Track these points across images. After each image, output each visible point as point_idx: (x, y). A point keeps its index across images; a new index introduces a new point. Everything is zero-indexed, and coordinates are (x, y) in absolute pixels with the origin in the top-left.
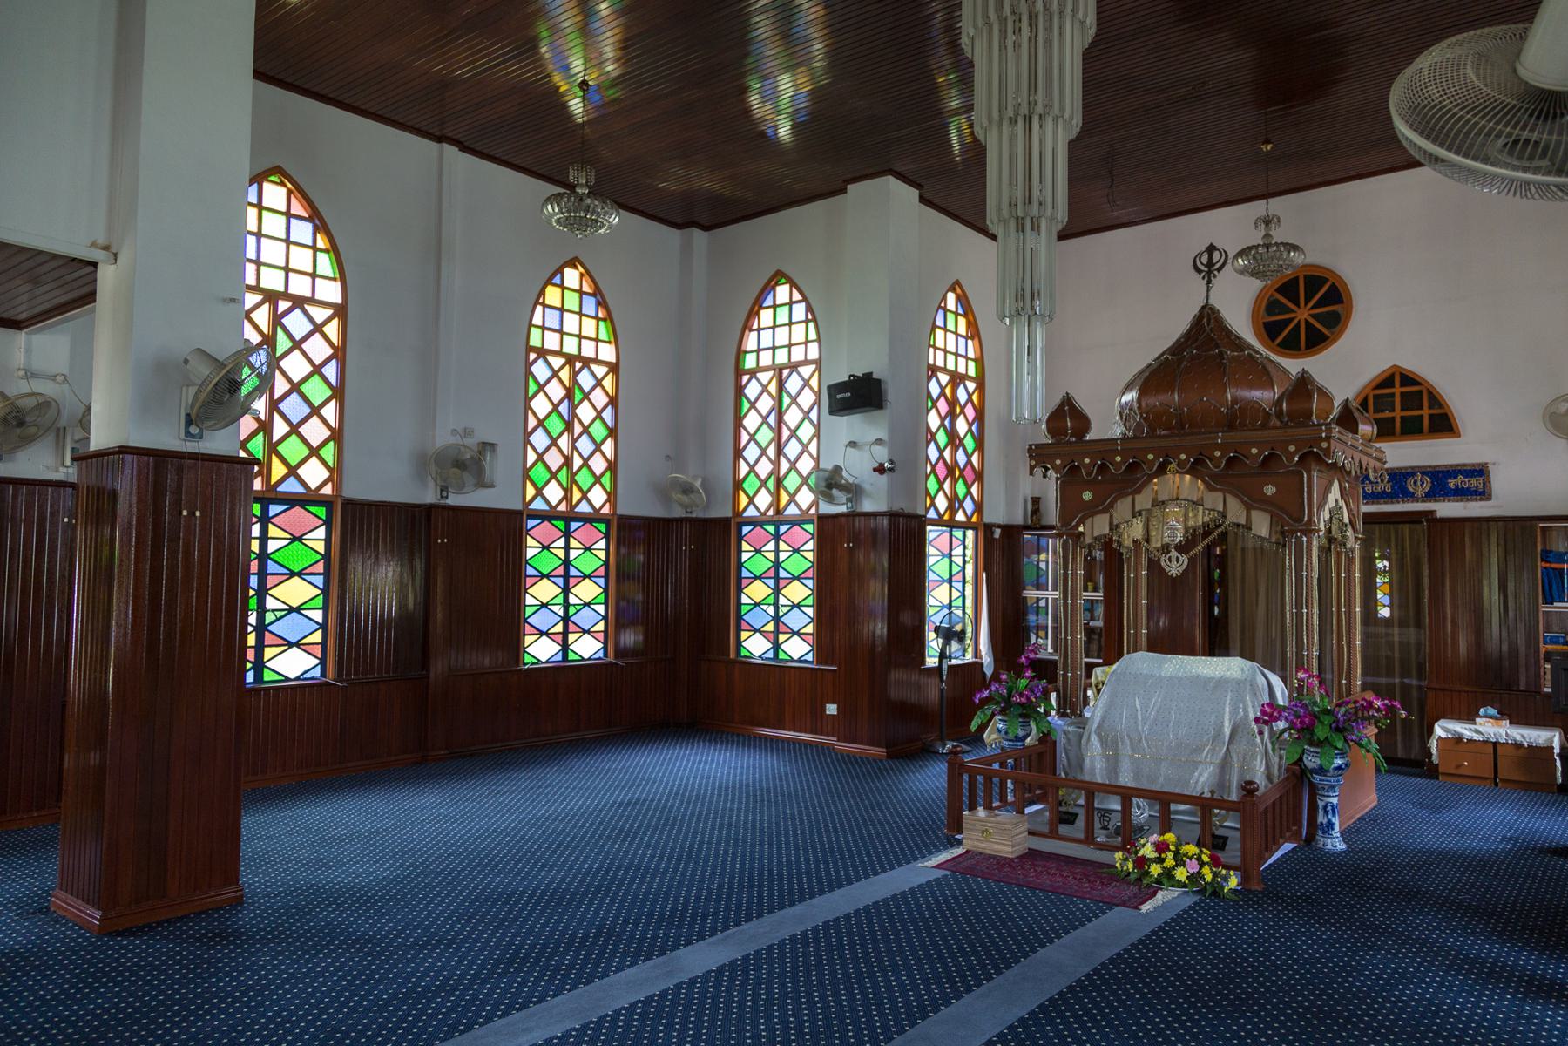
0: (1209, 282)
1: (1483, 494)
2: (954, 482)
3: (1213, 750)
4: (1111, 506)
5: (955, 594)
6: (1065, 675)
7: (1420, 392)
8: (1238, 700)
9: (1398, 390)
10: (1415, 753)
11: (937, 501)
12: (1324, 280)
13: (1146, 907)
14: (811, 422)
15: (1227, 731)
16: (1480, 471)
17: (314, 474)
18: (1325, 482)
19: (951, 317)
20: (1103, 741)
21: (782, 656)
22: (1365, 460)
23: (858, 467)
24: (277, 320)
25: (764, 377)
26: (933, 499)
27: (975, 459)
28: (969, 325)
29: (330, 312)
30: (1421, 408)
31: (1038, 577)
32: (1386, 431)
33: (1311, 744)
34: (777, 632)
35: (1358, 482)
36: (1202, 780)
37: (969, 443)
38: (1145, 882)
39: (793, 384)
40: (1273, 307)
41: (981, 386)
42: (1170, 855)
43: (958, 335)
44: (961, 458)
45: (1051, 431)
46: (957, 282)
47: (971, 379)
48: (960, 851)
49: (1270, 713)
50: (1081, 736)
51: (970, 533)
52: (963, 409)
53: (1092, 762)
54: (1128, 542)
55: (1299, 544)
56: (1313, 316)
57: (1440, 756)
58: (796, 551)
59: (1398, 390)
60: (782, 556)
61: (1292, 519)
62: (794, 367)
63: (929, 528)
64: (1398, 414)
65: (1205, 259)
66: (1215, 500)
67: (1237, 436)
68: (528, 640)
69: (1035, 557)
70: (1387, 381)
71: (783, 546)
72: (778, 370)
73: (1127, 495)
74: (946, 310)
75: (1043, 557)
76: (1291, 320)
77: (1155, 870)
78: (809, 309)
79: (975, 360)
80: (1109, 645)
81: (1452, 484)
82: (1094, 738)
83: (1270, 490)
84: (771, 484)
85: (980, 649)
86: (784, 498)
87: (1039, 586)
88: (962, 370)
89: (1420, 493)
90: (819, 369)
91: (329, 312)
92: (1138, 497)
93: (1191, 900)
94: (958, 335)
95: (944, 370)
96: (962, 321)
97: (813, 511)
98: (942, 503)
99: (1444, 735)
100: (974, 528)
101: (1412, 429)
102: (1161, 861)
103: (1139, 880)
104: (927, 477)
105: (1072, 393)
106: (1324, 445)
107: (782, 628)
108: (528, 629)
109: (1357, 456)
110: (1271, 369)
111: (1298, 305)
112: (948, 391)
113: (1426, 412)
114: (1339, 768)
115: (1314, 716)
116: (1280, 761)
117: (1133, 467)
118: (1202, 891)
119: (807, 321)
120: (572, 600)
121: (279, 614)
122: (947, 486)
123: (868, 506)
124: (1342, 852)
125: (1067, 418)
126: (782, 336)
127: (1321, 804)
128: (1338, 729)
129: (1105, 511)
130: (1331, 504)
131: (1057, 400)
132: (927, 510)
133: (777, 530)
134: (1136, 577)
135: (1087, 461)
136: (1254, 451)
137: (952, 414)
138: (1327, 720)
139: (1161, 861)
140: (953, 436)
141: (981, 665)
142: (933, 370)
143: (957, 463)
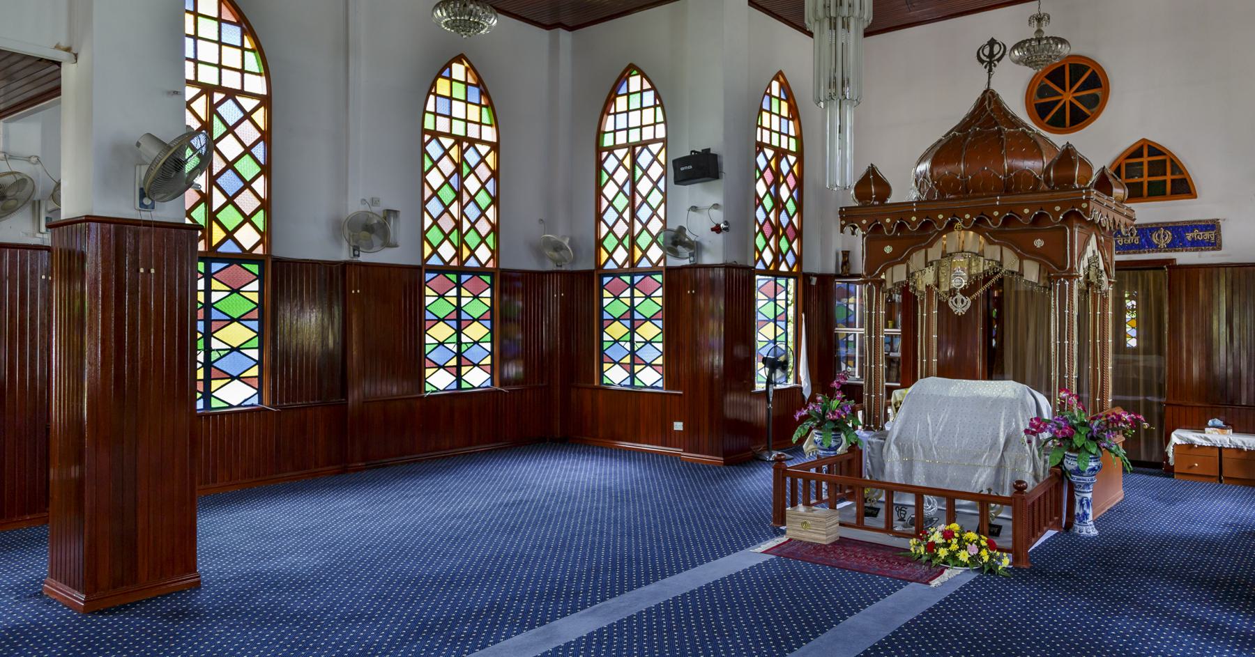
0: (990, 70)
1: (1216, 245)
2: (778, 239)
3: (990, 456)
4: (908, 257)
5: (779, 331)
6: (869, 397)
8: (1012, 415)
9: (1145, 159)
14: (659, 190)
15: (1002, 440)
16: (1213, 226)
17: (248, 237)
19: (775, 102)
21: (637, 383)
22: (1118, 217)
23: (699, 227)
24: (213, 109)
25: (620, 153)
26: (761, 254)
27: (795, 220)
29: (256, 102)
32: (1136, 193)
33: (1070, 450)
34: (633, 363)
35: (1110, 235)
36: (981, 480)
37: (791, 207)
40: (1043, 91)
42: (955, 541)
44: (784, 219)
46: (780, 73)
48: (784, 539)
50: (882, 446)
53: (892, 466)
54: (922, 288)
57: (1175, 458)
58: (648, 297)
60: (637, 301)
61: (1056, 266)
62: (645, 144)
64: (1146, 179)
65: (987, 51)
66: (993, 252)
67: (1013, 199)
68: (428, 372)
69: (845, 300)
70: (1136, 152)
71: (637, 293)
72: (631, 147)
73: (921, 248)
74: (771, 96)
75: (851, 300)
77: (943, 553)
78: (657, 96)
81: (1189, 236)
82: (893, 447)
83: (1039, 243)
88: (784, 146)
89: (1163, 245)
90: (665, 146)
91: (256, 102)
95: (770, 146)
96: (784, 105)
97: (661, 264)
98: (768, 256)
101: (1157, 192)
102: (947, 545)
104: (756, 235)
106: (1084, 205)
107: (637, 360)
108: (428, 363)
109: (1111, 215)
110: (1041, 143)
112: (773, 163)
113: (1169, 177)
114: (1093, 469)
115: (1074, 427)
116: (1045, 464)
117: (926, 226)
119: (655, 106)
120: (464, 339)
121: (222, 353)
122: (772, 243)
123: (707, 259)
125: (872, 184)
126: (635, 119)
127: (1078, 499)
129: (903, 262)
130: (1089, 254)
131: (863, 171)
132: (756, 262)
134: (928, 317)
136: (1026, 211)
138: (1084, 431)
139: (947, 545)
142: (761, 146)
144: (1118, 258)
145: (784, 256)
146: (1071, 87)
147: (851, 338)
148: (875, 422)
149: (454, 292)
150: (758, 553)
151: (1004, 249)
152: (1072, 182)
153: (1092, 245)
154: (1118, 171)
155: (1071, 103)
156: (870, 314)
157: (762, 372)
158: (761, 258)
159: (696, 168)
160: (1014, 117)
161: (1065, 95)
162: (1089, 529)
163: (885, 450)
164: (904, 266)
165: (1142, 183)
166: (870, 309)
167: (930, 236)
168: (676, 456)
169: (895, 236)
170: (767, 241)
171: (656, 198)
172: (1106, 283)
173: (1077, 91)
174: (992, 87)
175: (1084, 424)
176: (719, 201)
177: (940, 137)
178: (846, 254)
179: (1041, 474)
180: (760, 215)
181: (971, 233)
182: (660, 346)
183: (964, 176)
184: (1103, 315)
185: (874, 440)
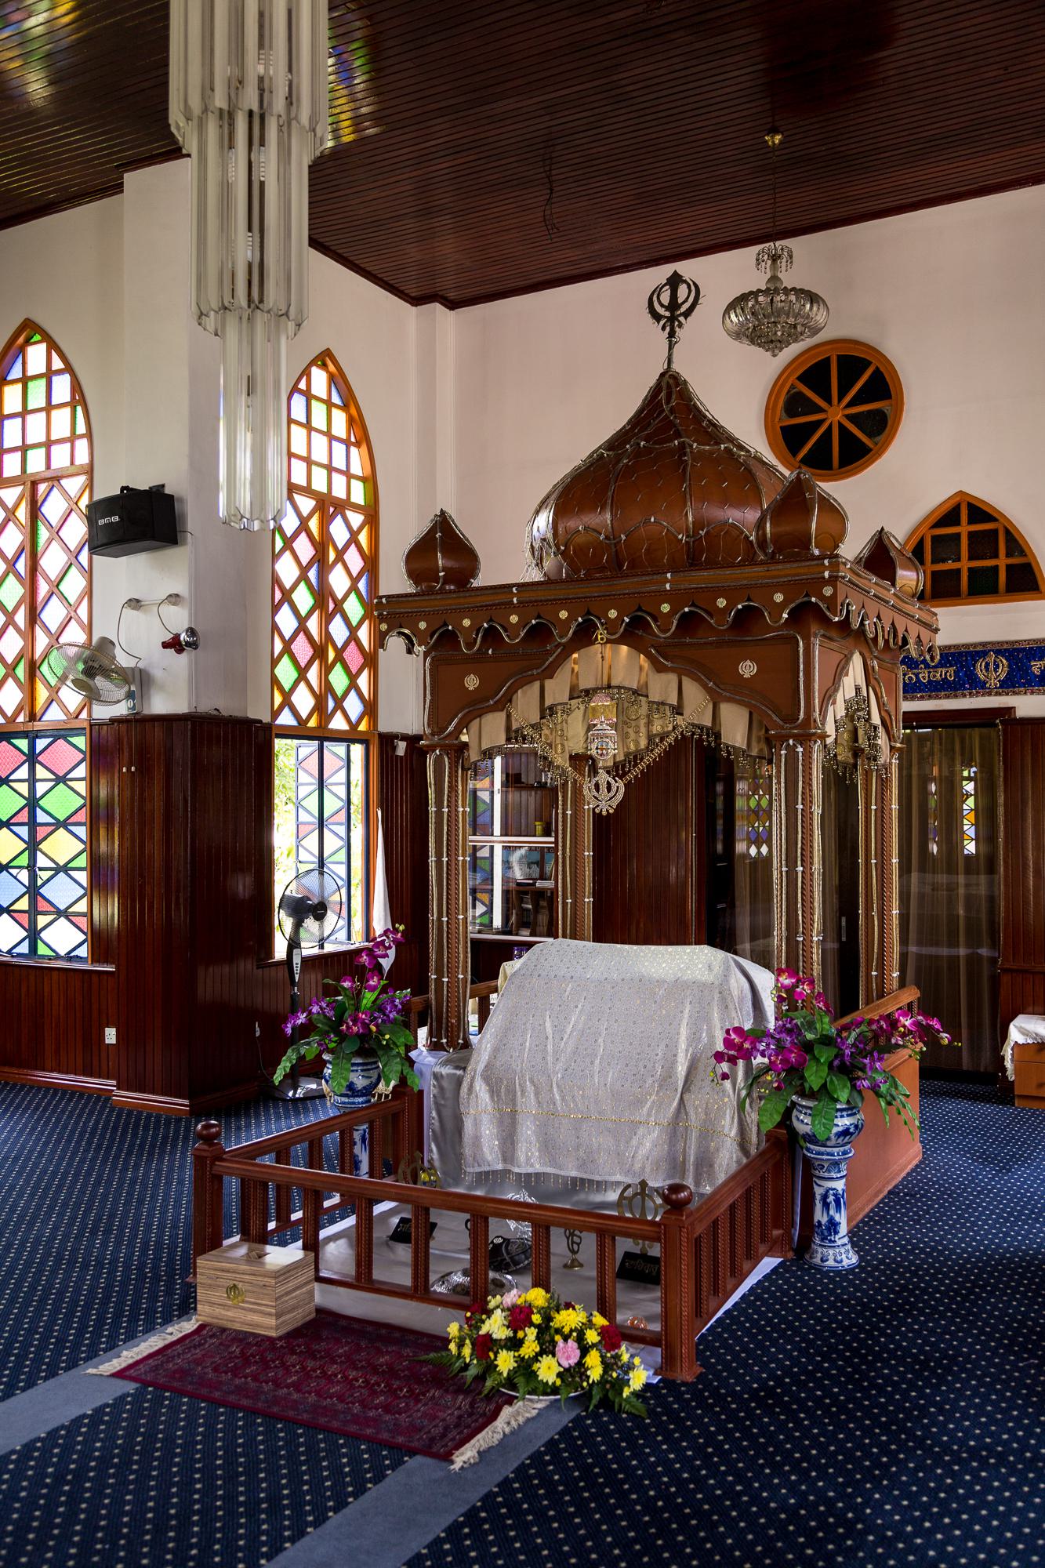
0: (672, 334)
2: (327, 669)
3: (660, 1105)
4: (509, 699)
5: (332, 843)
6: (438, 981)
7: (995, 532)
8: (701, 1017)
9: (964, 529)
10: (985, 1062)
11: (295, 699)
13: (465, 1455)
15: (681, 1069)
18: (836, 657)
19: (319, 409)
20: (493, 1092)
21: (42, 950)
22: (901, 623)
23: (138, 641)
26: (287, 696)
30: (996, 556)
32: (943, 589)
33: (802, 1094)
34: (34, 911)
35: (891, 653)
36: (643, 1152)
38: (489, 1383)
39: (53, 507)
40: (795, 404)
42: (531, 1333)
43: (331, 438)
44: (338, 631)
46: (327, 353)
47: (356, 508)
48: (188, 1326)
49: (738, 1046)
50: (459, 1081)
51: (357, 750)
52: (340, 555)
53: (477, 1123)
55: (792, 756)
56: (848, 417)
57: (1016, 1071)
58: (61, 779)
59: (964, 529)
60: (41, 788)
61: (783, 718)
62: (55, 479)
63: (279, 744)
64: (965, 564)
65: (665, 298)
66: (664, 686)
67: (700, 578)
70: (949, 515)
71: (41, 773)
73: (530, 681)
74: (308, 396)
76: (820, 422)
77: (505, 1362)
78: (76, 387)
79: (363, 479)
82: (480, 1087)
83: (748, 669)
84: (21, 671)
86: (42, 694)
88: (339, 492)
89: (993, 682)
92: (548, 683)
93: (565, 1418)
94: (331, 438)
95: (307, 491)
96: (340, 419)
97: (84, 715)
98: (304, 701)
99: (1021, 1040)
100: (364, 741)
101: (983, 587)
102: (514, 1344)
103: (481, 1378)
104: (275, 662)
106: (828, 591)
107: (42, 905)
109: (888, 616)
110: (760, 474)
111: (829, 401)
112: (314, 525)
113: (1002, 562)
114: (846, 1132)
115: (808, 1047)
116: (761, 1119)
117: (540, 633)
118: (587, 1396)
122: (313, 675)
123: (160, 705)
124: (851, 1270)
125: (443, 549)
127: (819, 1192)
128: (846, 1069)
130: (844, 691)
132: (276, 714)
133: (32, 746)
135: (467, 623)
136: (722, 603)
137: (320, 559)
138: (825, 1055)
139: (514, 1344)
140: (322, 594)
143: (329, 638)
144: (908, 706)
146: (840, 400)
148: (452, 1039)
149: (23, 773)
150: (105, 1374)
151: (686, 681)
152: (806, 545)
153: (855, 675)
154: (918, 551)
155: (841, 426)
157: (284, 922)
158: (287, 702)
159: (138, 520)
160: (713, 424)
161: (831, 410)
162: (841, 1255)
165: (958, 571)
167: (549, 653)
168: (104, 1096)
170: (353, 678)
171: (74, 585)
172: (886, 750)
173: (848, 406)
174: (676, 367)
175: (826, 1041)
176: (181, 587)
177: (578, 462)
179: (754, 1139)
180: (286, 621)
181: (624, 649)
182: (83, 877)
183: (613, 536)
184: (882, 811)
185: (446, 1070)
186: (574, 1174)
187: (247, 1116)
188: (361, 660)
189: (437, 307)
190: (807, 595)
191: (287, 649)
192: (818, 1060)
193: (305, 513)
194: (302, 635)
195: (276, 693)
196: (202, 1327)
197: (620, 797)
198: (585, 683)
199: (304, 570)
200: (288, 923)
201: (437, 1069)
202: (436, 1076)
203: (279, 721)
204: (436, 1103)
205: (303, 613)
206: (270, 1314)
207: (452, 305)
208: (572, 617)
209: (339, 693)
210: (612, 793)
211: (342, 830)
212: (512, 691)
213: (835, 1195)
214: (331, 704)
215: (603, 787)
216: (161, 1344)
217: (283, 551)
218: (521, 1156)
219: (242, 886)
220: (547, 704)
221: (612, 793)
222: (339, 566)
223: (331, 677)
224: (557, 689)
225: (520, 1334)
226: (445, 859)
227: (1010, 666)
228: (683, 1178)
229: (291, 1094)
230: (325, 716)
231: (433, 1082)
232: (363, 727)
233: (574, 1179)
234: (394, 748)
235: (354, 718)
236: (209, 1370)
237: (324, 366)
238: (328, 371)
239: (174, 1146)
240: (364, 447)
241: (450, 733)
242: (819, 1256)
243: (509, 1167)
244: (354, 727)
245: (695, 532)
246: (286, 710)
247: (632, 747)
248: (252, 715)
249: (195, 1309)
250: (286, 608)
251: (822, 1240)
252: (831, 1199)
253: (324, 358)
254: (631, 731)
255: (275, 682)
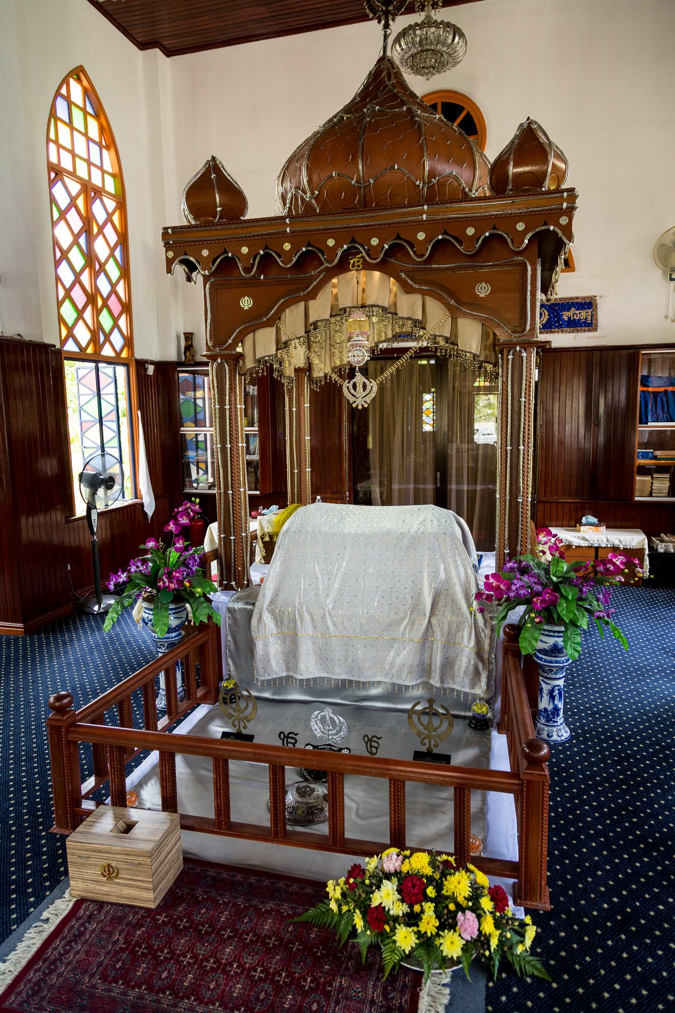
1: (590, 325)
2: (97, 312)
4: (278, 317)
5: (108, 434)
11: (76, 332)
12: (460, 109)
16: (588, 304)
20: (278, 619)
26: (70, 330)
28: (102, 129)
31: (196, 413)
36: (399, 660)
37: (113, 271)
41: (122, 206)
42: (429, 908)
44: (104, 286)
45: (193, 209)
50: (250, 614)
53: (266, 646)
54: (289, 372)
63: (66, 363)
66: (410, 305)
69: (191, 394)
73: (296, 301)
75: (199, 394)
77: (405, 939)
79: (113, 175)
80: (272, 490)
81: (566, 315)
82: (267, 617)
85: (135, 488)
87: (197, 423)
88: (96, 180)
92: (311, 303)
98: (83, 335)
100: (126, 365)
102: (412, 919)
104: (60, 304)
105: (219, 158)
115: (556, 587)
117: (307, 260)
122: (88, 314)
125: (213, 190)
127: (546, 688)
129: (269, 324)
131: (196, 169)
132: (63, 342)
134: (299, 412)
136: (470, 231)
137: (87, 228)
139: (412, 919)
140: (90, 258)
141: (142, 505)
142: (57, 173)
143: (97, 290)
145: (107, 337)
147: (201, 438)
156: (224, 449)
158: (70, 334)
163: (254, 621)
164: (273, 329)
166: (222, 402)
167: (313, 278)
169: (255, 278)
170: (116, 320)
177: (316, 129)
178: (189, 336)
180: (67, 277)
181: (377, 274)
185: (239, 606)
186: (343, 677)
187: (69, 631)
188: (120, 308)
189: (157, 51)
190: (546, 224)
191: (68, 295)
192: (566, 598)
193: (74, 194)
194: (77, 285)
195: (63, 327)
196: (79, 903)
197: (373, 395)
198: (344, 303)
199: (76, 237)
200: (86, 491)
201: (231, 605)
202: (230, 610)
203: (66, 348)
204: (231, 630)
205: (78, 270)
206: (147, 889)
207: (169, 53)
208: (338, 245)
209: (107, 331)
210: (366, 393)
211: (114, 426)
212: (282, 309)
213: (559, 690)
214: (102, 338)
215: (360, 388)
216: (38, 942)
217: (59, 220)
218: (302, 666)
219: (48, 466)
220: (312, 319)
221: (366, 393)
222: (101, 237)
223: (100, 318)
224: (319, 308)
225: (417, 908)
226: (229, 446)
227: (549, 315)
228: (429, 677)
229: (96, 608)
230: (98, 347)
231: (228, 615)
232: (124, 355)
233: (344, 681)
234: (146, 370)
235: (118, 349)
236: (96, 980)
237: (79, 80)
238: (82, 86)
239: (16, 666)
240: (112, 151)
241: (230, 345)
242: (545, 733)
243: (291, 674)
244: (118, 354)
245: (430, 182)
246: (71, 340)
247: (338, 363)
248: (48, 340)
249: (66, 873)
250: (64, 263)
251: (548, 721)
252: (556, 692)
253: (78, 73)
254: (336, 351)
255: (61, 319)
